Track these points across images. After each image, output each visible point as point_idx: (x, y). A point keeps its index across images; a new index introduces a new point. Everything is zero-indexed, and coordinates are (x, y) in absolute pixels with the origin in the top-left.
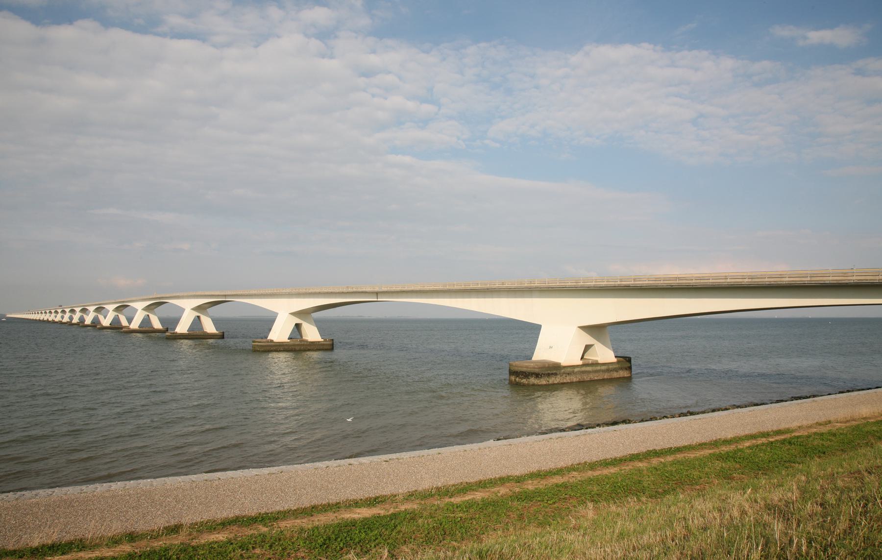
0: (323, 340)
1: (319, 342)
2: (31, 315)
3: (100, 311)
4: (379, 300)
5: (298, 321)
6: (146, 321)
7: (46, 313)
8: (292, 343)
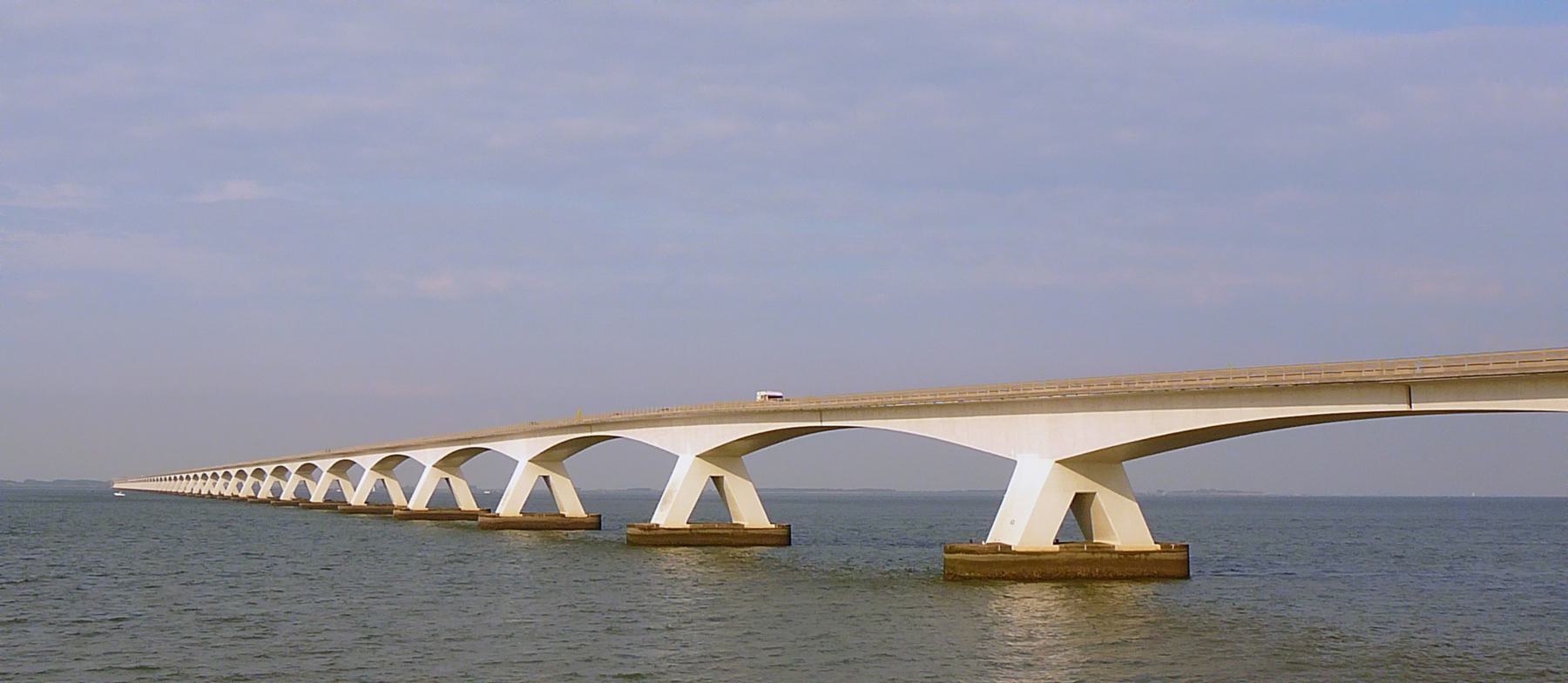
0: (1158, 547)
1: (1147, 553)
2: (156, 482)
3: (391, 469)
4: (1415, 407)
5: (1084, 485)
6: (542, 497)
7: (215, 476)
8: (1065, 555)
